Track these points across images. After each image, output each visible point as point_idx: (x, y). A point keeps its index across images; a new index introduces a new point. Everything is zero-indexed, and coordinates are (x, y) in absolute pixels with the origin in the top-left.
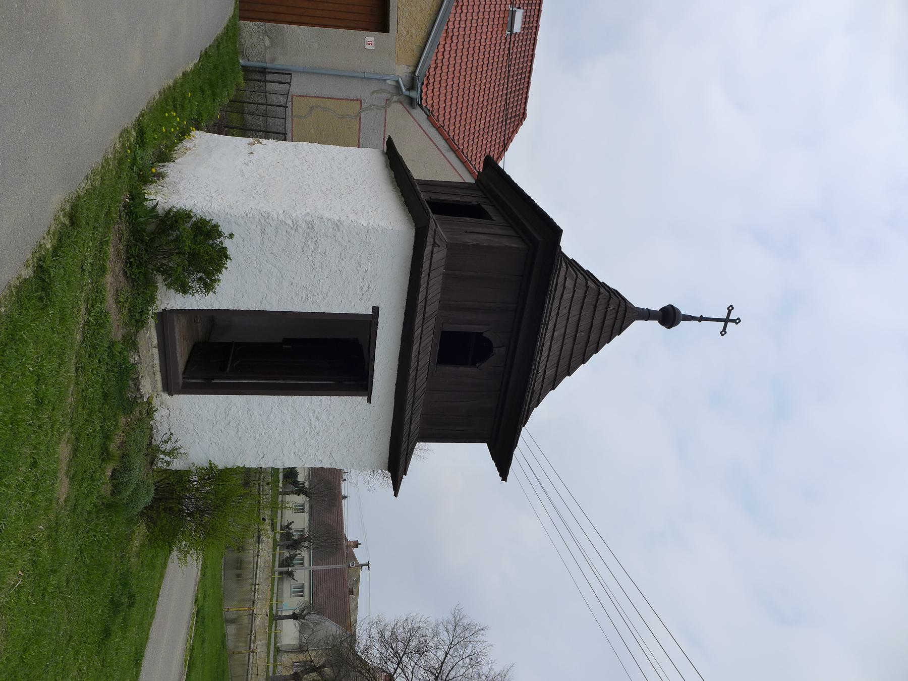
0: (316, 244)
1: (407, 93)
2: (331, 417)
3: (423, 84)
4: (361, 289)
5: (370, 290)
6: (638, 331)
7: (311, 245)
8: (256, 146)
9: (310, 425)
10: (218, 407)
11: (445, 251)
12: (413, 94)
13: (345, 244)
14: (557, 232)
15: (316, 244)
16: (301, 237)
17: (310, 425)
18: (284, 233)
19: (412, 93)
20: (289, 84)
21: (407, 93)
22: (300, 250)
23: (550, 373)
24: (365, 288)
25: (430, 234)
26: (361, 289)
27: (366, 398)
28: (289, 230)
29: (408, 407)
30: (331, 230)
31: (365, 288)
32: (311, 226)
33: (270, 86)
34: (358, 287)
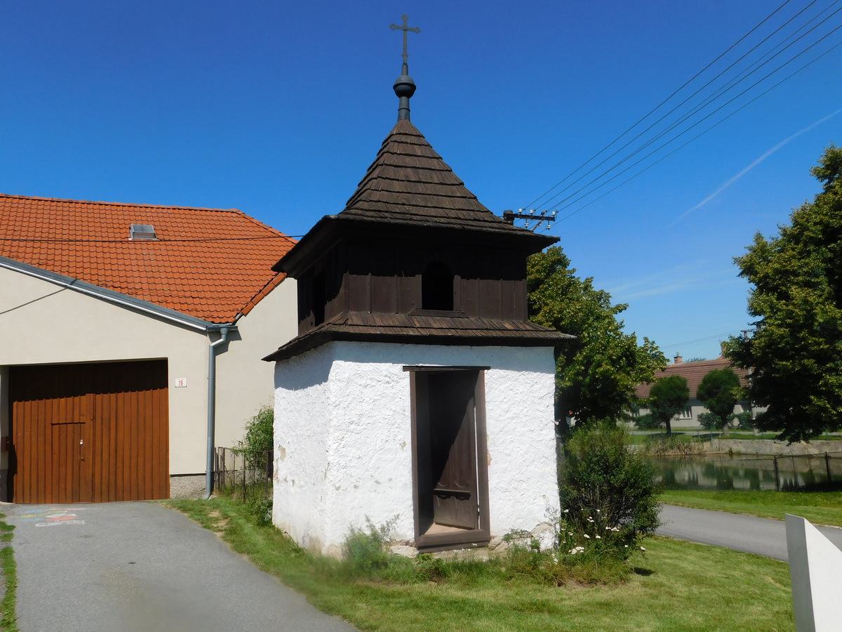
0: (500, 415)
1: (223, 336)
2: (505, 400)
3: (213, 322)
4: (388, 382)
5: (389, 375)
6: (419, 121)
7: (353, 427)
8: (279, 477)
9: (513, 418)
10: (500, 499)
11: (352, 313)
12: (223, 331)
13: (350, 399)
14: (326, 220)
15: (351, 423)
16: (346, 436)
17: (513, 418)
18: (344, 449)
19: (222, 335)
20: (224, 449)
21: (223, 336)
22: (358, 436)
23: (460, 203)
24: (387, 379)
25: (335, 329)
26: (388, 382)
27: (486, 371)
28: (342, 446)
29: (495, 334)
30: (340, 412)
31: (387, 379)
32: (623, 431)
33: (228, 468)
34: (387, 385)
